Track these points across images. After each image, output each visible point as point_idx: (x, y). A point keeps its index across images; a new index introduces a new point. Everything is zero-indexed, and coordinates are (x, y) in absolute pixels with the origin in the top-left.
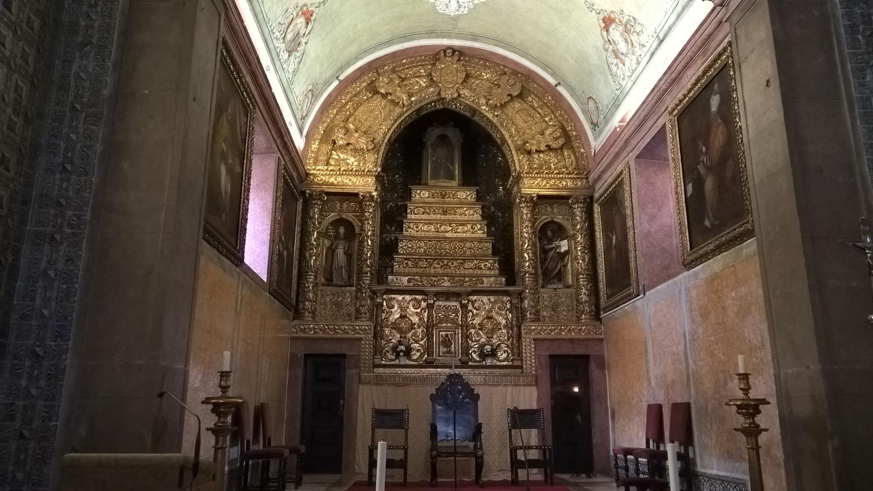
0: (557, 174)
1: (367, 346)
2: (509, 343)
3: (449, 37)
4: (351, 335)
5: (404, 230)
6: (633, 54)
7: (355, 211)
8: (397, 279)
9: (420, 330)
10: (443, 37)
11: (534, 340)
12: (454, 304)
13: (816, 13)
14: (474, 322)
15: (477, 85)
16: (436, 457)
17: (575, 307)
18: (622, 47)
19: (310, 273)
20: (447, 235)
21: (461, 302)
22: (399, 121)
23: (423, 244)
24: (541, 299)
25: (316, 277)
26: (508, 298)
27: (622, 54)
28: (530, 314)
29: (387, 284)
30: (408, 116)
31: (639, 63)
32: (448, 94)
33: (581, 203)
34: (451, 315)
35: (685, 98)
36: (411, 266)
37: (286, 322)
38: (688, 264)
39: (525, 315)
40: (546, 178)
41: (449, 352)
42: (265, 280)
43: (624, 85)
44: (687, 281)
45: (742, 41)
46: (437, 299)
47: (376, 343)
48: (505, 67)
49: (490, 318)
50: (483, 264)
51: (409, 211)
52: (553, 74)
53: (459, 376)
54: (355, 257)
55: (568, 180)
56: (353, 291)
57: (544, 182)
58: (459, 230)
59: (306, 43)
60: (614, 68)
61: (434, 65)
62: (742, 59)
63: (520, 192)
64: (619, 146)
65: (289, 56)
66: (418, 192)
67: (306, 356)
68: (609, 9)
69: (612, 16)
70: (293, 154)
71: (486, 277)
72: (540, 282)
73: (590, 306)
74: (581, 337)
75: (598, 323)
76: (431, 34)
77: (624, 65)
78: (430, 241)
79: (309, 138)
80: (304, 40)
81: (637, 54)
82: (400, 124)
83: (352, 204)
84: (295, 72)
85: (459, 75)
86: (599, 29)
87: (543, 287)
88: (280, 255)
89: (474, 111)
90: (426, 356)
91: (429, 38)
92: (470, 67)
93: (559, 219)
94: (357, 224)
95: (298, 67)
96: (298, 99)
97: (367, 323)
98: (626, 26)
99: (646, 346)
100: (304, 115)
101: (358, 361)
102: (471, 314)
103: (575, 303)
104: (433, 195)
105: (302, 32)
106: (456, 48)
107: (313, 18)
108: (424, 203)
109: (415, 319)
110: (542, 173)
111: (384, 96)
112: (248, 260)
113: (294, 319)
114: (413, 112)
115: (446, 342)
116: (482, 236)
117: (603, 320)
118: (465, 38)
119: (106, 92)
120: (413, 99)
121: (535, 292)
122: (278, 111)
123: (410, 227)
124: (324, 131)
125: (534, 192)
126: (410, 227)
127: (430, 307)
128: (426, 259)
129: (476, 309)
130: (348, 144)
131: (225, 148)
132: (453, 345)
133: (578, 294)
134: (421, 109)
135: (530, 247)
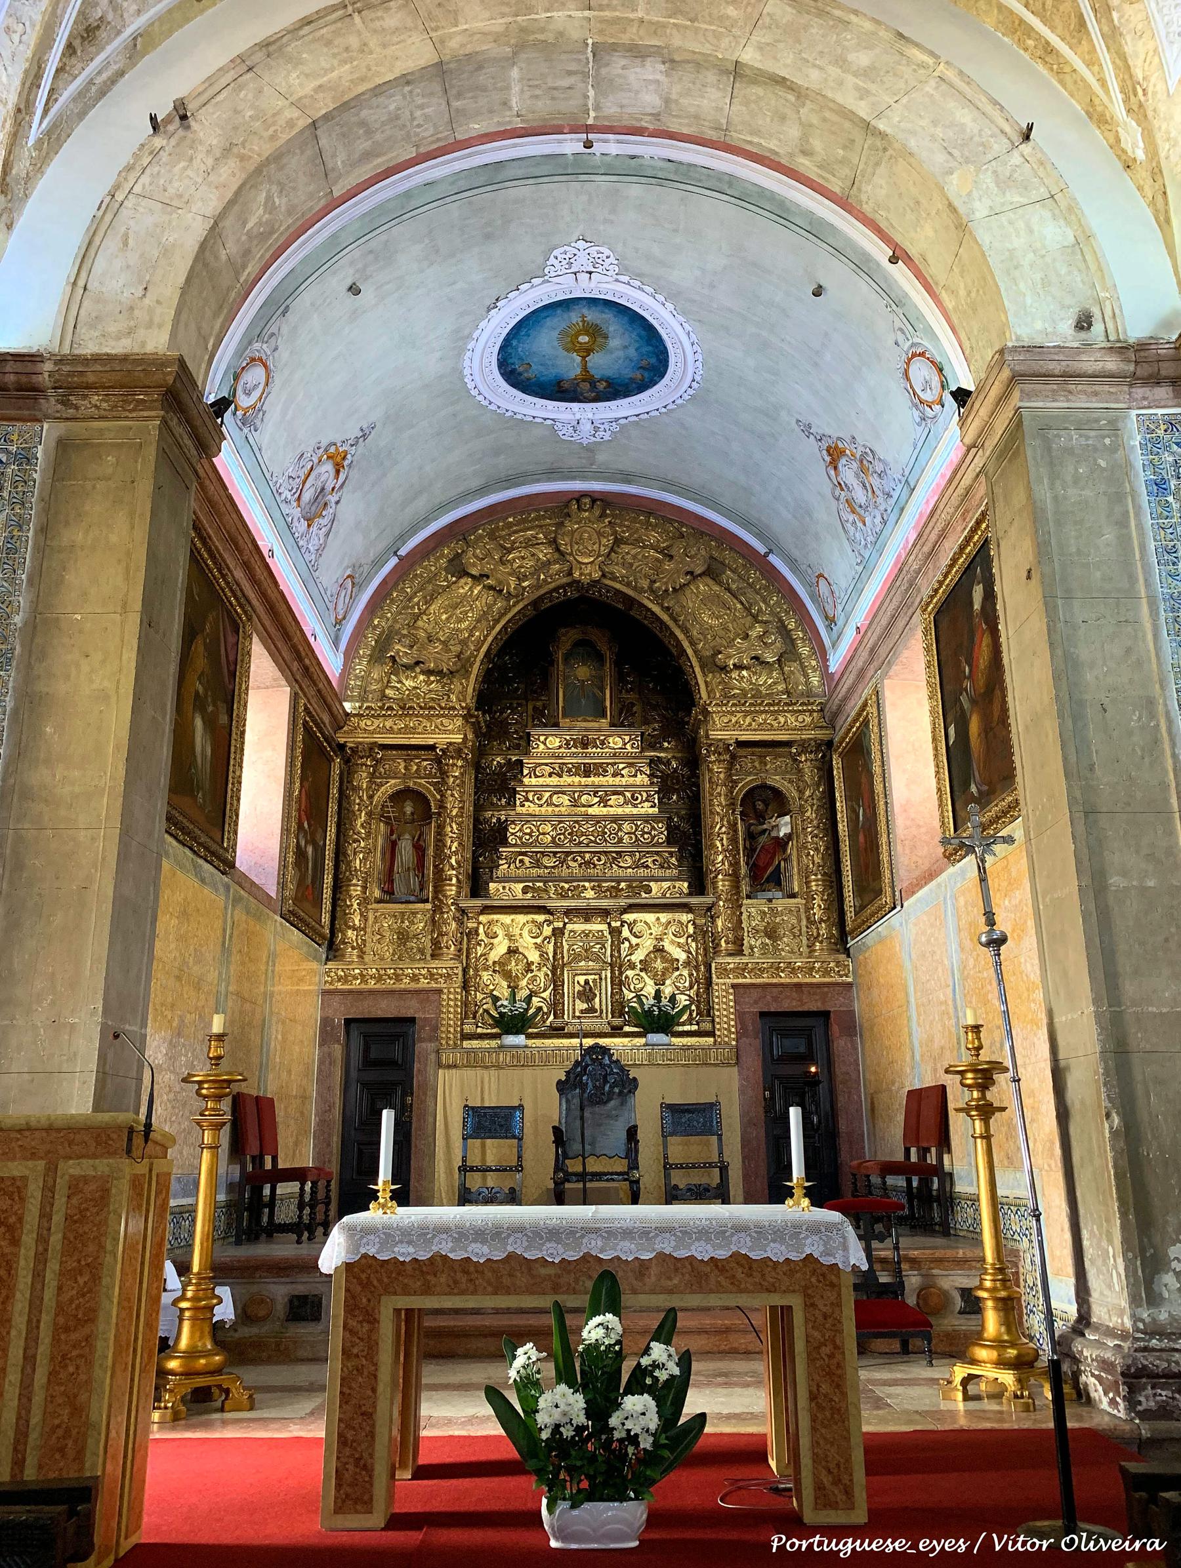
0: (769, 705)
1: (452, 1003)
2: (692, 993)
3: (584, 478)
4: (423, 983)
5: (518, 803)
6: (876, 507)
7: (430, 776)
8: (504, 888)
9: (541, 975)
10: (574, 478)
11: (734, 986)
12: (598, 926)
13: (1103, 463)
14: (633, 958)
15: (634, 557)
16: (563, 1183)
17: (804, 929)
18: (860, 496)
19: (354, 881)
20: (590, 811)
21: (609, 924)
22: (503, 622)
23: (549, 828)
24: (744, 917)
25: (365, 888)
26: (690, 916)
27: (861, 506)
28: (727, 942)
29: (487, 895)
30: (519, 612)
31: (884, 522)
32: (587, 568)
33: (811, 752)
34: (592, 947)
35: (941, 587)
36: (528, 865)
37: (314, 965)
38: (951, 855)
39: (719, 945)
40: (751, 712)
41: (592, 1010)
42: (273, 895)
43: (867, 557)
44: (952, 882)
45: (1000, 504)
46: (571, 920)
47: (467, 997)
48: (682, 524)
49: (659, 950)
50: (650, 860)
51: (526, 772)
52: (760, 536)
53: (605, 1050)
54: (431, 851)
55: (788, 715)
56: (428, 910)
57: (748, 720)
58: (609, 803)
59: (337, 503)
60: (852, 529)
61: (561, 525)
62: (1000, 534)
63: (707, 736)
64: (862, 659)
65: (309, 526)
66: (542, 738)
67: (348, 1022)
68: (835, 435)
69: (840, 445)
70: (321, 686)
71: (656, 881)
72: (745, 888)
73: (829, 928)
74: (814, 980)
75: (842, 957)
76: (552, 473)
77: (865, 524)
78: (560, 822)
79: (350, 656)
80: (333, 499)
81: (882, 508)
82: (505, 627)
83: (425, 763)
84: (320, 551)
85: (604, 541)
86: (823, 465)
87: (748, 897)
88: (300, 854)
89: (630, 602)
90: (552, 1017)
91: (549, 480)
92: (620, 526)
93: (776, 781)
94: (433, 796)
95: (325, 542)
96: (329, 593)
97: (451, 964)
98: (861, 462)
99: (907, 994)
100: (340, 617)
101: (436, 1029)
102: (627, 944)
103: (804, 922)
104: (567, 744)
105: (329, 487)
106: (596, 496)
107: (346, 463)
108: (554, 756)
109: (534, 956)
110: (744, 704)
111: (477, 579)
112: (243, 860)
113: (328, 959)
114: (526, 606)
115: (587, 994)
116: (651, 811)
117: (851, 951)
118: (611, 479)
119: (18, 619)
120: (526, 584)
121: (736, 906)
122: (291, 619)
123: (527, 800)
124: (376, 642)
125: (729, 735)
126: (527, 800)
127: (558, 933)
128: (555, 853)
129: (636, 937)
130: (417, 663)
131: (201, 689)
132: (597, 1000)
133: (808, 909)
134: (541, 598)
135: (724, 829)
